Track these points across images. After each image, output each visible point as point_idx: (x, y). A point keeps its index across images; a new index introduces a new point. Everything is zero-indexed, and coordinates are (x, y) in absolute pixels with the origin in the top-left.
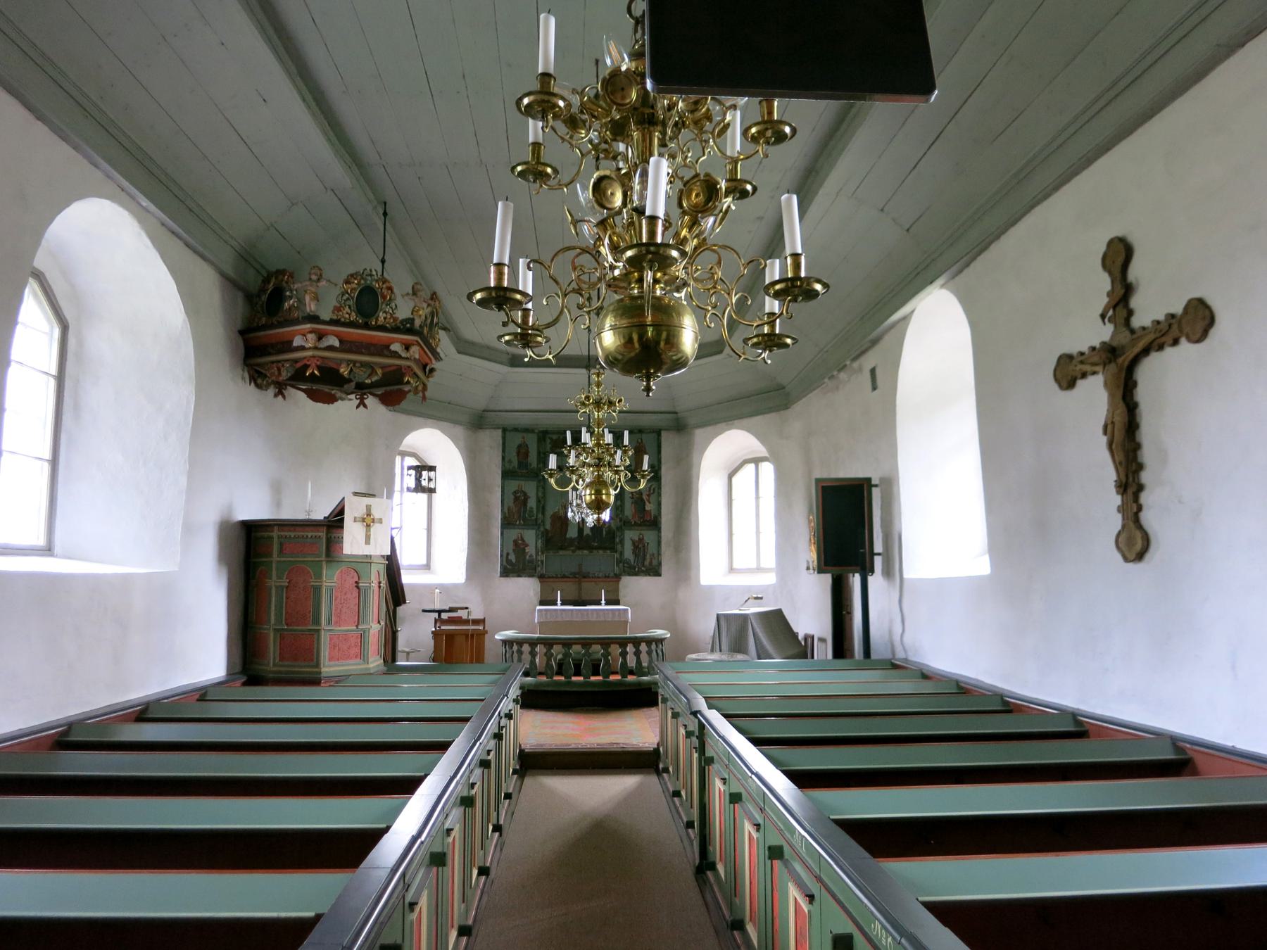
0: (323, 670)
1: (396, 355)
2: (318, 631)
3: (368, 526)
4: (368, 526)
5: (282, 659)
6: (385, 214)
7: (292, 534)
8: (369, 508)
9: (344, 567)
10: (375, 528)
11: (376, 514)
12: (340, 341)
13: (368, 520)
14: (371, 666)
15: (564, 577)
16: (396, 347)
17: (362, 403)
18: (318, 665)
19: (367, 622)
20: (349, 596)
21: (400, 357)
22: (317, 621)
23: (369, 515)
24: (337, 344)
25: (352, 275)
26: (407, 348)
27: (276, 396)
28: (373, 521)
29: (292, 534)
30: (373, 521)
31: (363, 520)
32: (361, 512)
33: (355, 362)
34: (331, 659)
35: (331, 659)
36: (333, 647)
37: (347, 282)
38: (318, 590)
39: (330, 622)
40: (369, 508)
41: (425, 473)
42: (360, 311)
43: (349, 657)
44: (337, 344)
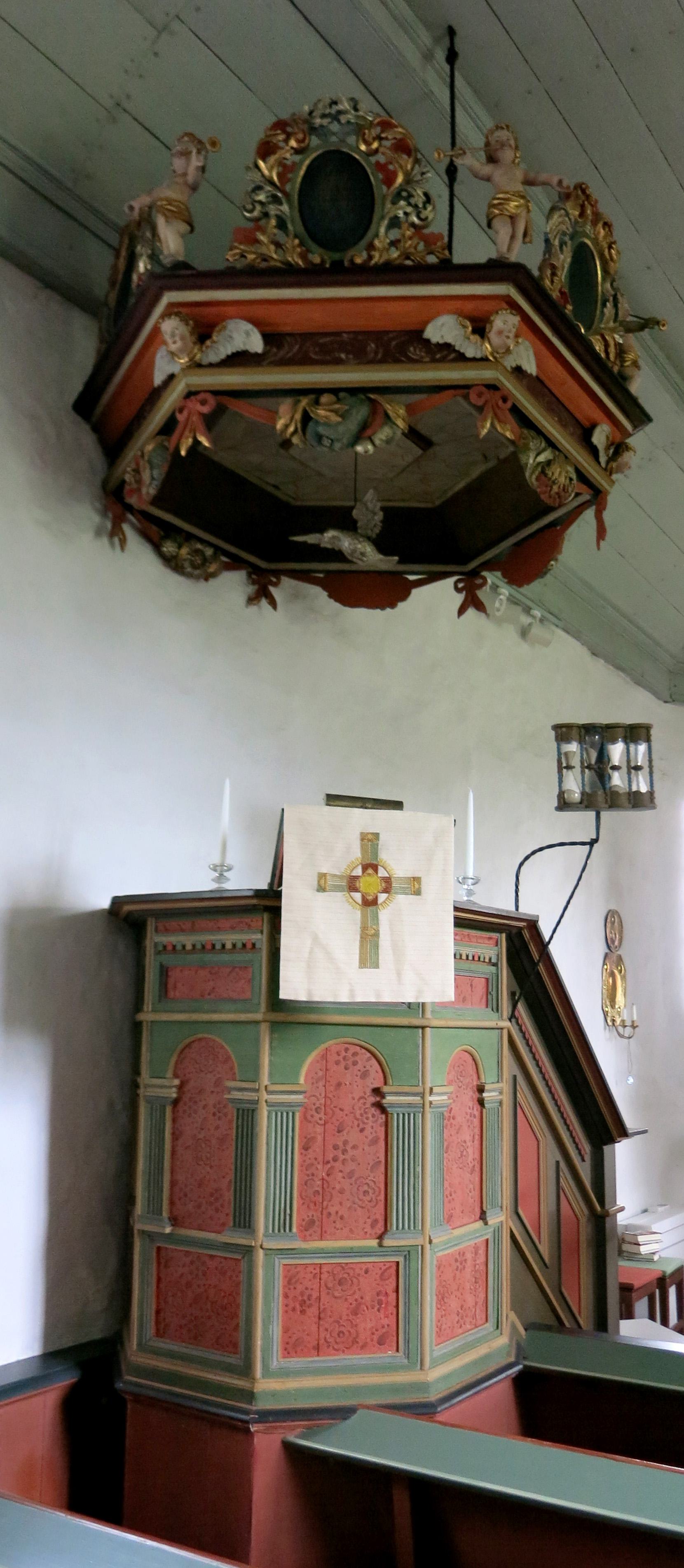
0: (263, 1385)
1: (446, 353)
2: (248, 1251)
3: (370, 903)
4: (370, 903)
5: (159, 1334)
6: (452, 57)
7: (188, 940)
8: (370, 841)
9: (331, 1042)
10: (395, 912)
11: (397, 862)
12: (267, 338)
13: (370, 884)
14: (433, 1375)
15: (125, 110)
16: (444, 329)
17: (472, 601)
18: (246, 1370)
19: (415, 1223)
20: (353, 1136)
21: (461, 357)
22: (244, 1218)
23: (371, 866)
24: (256, 344)
25: (280, 125)
26: (480, 328)
27: (252, 600)
28: (388, 885)
29: (188, 940)
30: (388, 885)
31: (352, 884)
32: (344, 856)
33: (316, 393)
34: (291, 1348)
35: (291, 1348)
36: (298, 1303)
37: (266, 150)
38: (247, 1116)
39: (284, 1225)
40: (370, 841)
41: (617, 751)
42: (315, 230)
43: (353, 1344)
44: (256, 344)
